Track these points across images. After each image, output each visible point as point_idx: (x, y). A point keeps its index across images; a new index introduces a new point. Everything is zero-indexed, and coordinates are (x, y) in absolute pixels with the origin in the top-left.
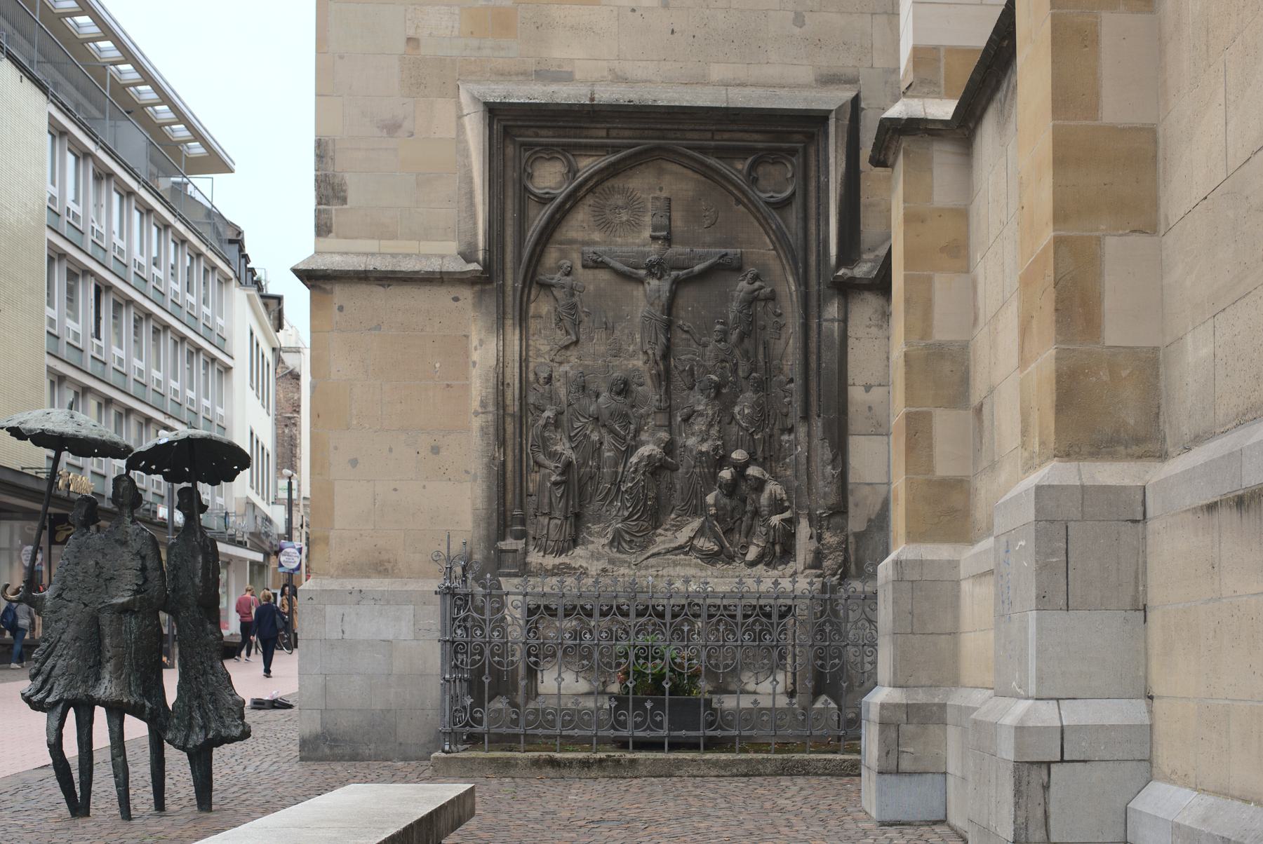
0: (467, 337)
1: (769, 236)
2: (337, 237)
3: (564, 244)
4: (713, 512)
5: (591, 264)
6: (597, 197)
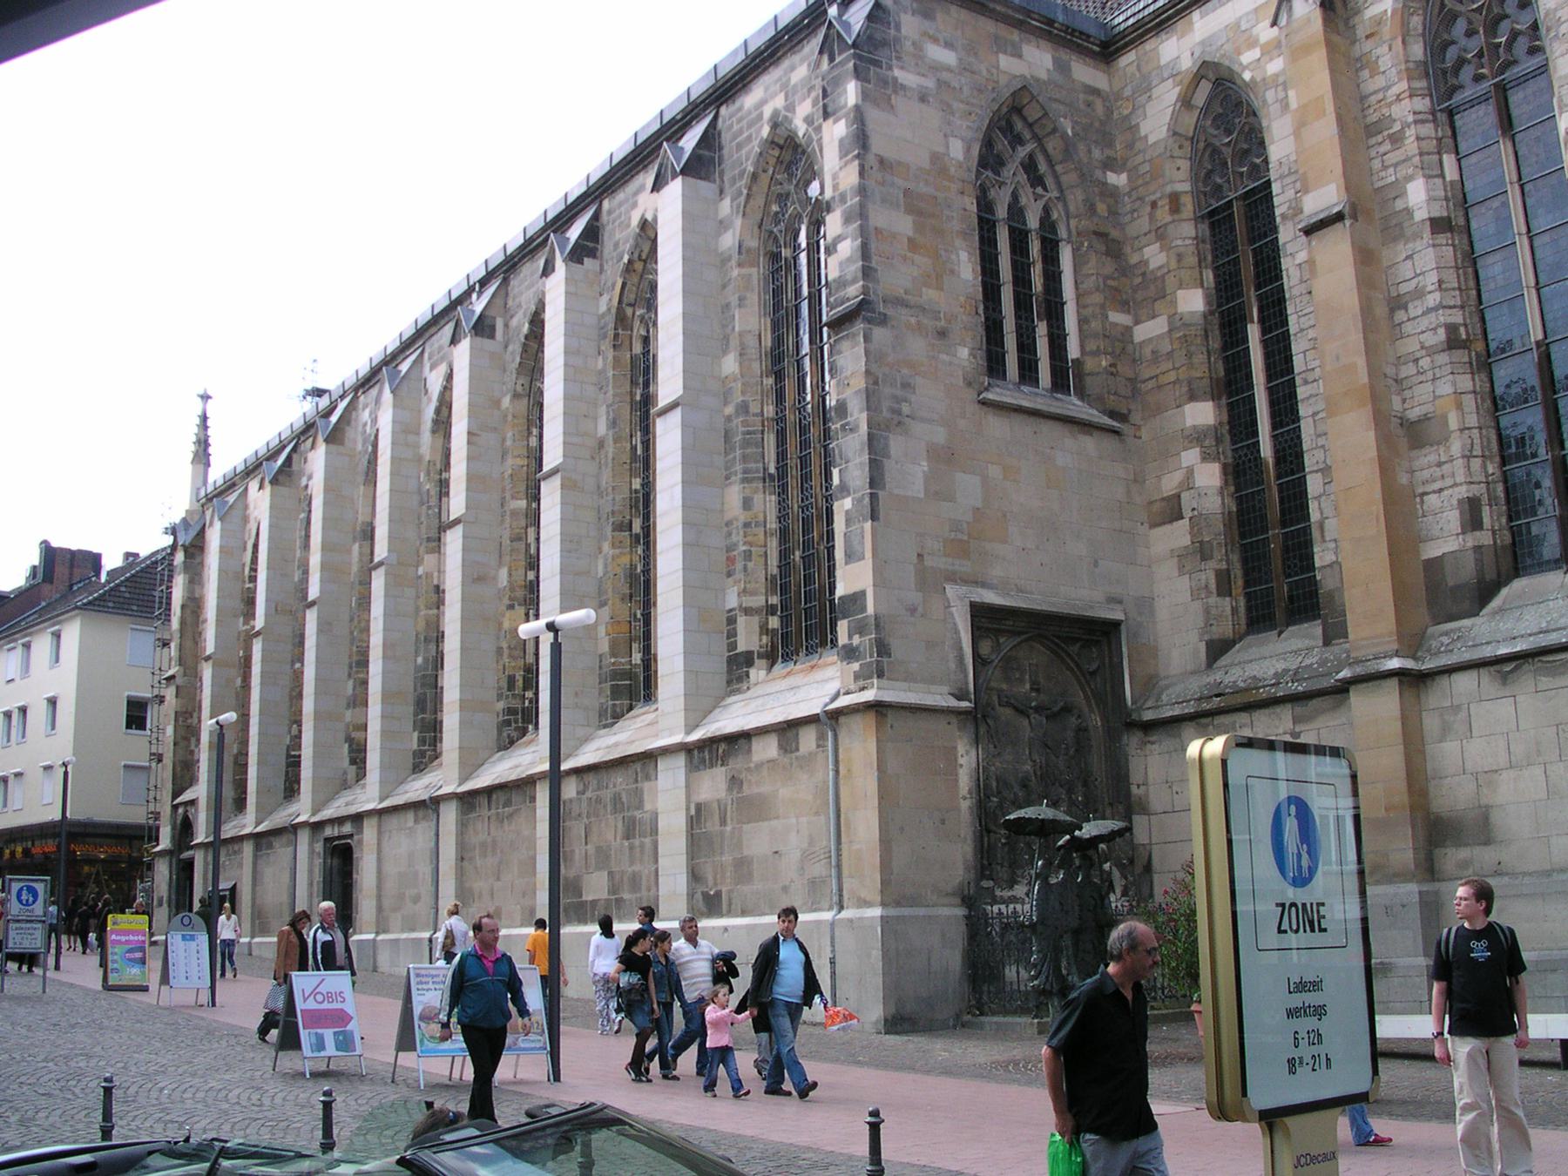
0: (955, 748)
1: (1084, 692)
2: (888, 679)
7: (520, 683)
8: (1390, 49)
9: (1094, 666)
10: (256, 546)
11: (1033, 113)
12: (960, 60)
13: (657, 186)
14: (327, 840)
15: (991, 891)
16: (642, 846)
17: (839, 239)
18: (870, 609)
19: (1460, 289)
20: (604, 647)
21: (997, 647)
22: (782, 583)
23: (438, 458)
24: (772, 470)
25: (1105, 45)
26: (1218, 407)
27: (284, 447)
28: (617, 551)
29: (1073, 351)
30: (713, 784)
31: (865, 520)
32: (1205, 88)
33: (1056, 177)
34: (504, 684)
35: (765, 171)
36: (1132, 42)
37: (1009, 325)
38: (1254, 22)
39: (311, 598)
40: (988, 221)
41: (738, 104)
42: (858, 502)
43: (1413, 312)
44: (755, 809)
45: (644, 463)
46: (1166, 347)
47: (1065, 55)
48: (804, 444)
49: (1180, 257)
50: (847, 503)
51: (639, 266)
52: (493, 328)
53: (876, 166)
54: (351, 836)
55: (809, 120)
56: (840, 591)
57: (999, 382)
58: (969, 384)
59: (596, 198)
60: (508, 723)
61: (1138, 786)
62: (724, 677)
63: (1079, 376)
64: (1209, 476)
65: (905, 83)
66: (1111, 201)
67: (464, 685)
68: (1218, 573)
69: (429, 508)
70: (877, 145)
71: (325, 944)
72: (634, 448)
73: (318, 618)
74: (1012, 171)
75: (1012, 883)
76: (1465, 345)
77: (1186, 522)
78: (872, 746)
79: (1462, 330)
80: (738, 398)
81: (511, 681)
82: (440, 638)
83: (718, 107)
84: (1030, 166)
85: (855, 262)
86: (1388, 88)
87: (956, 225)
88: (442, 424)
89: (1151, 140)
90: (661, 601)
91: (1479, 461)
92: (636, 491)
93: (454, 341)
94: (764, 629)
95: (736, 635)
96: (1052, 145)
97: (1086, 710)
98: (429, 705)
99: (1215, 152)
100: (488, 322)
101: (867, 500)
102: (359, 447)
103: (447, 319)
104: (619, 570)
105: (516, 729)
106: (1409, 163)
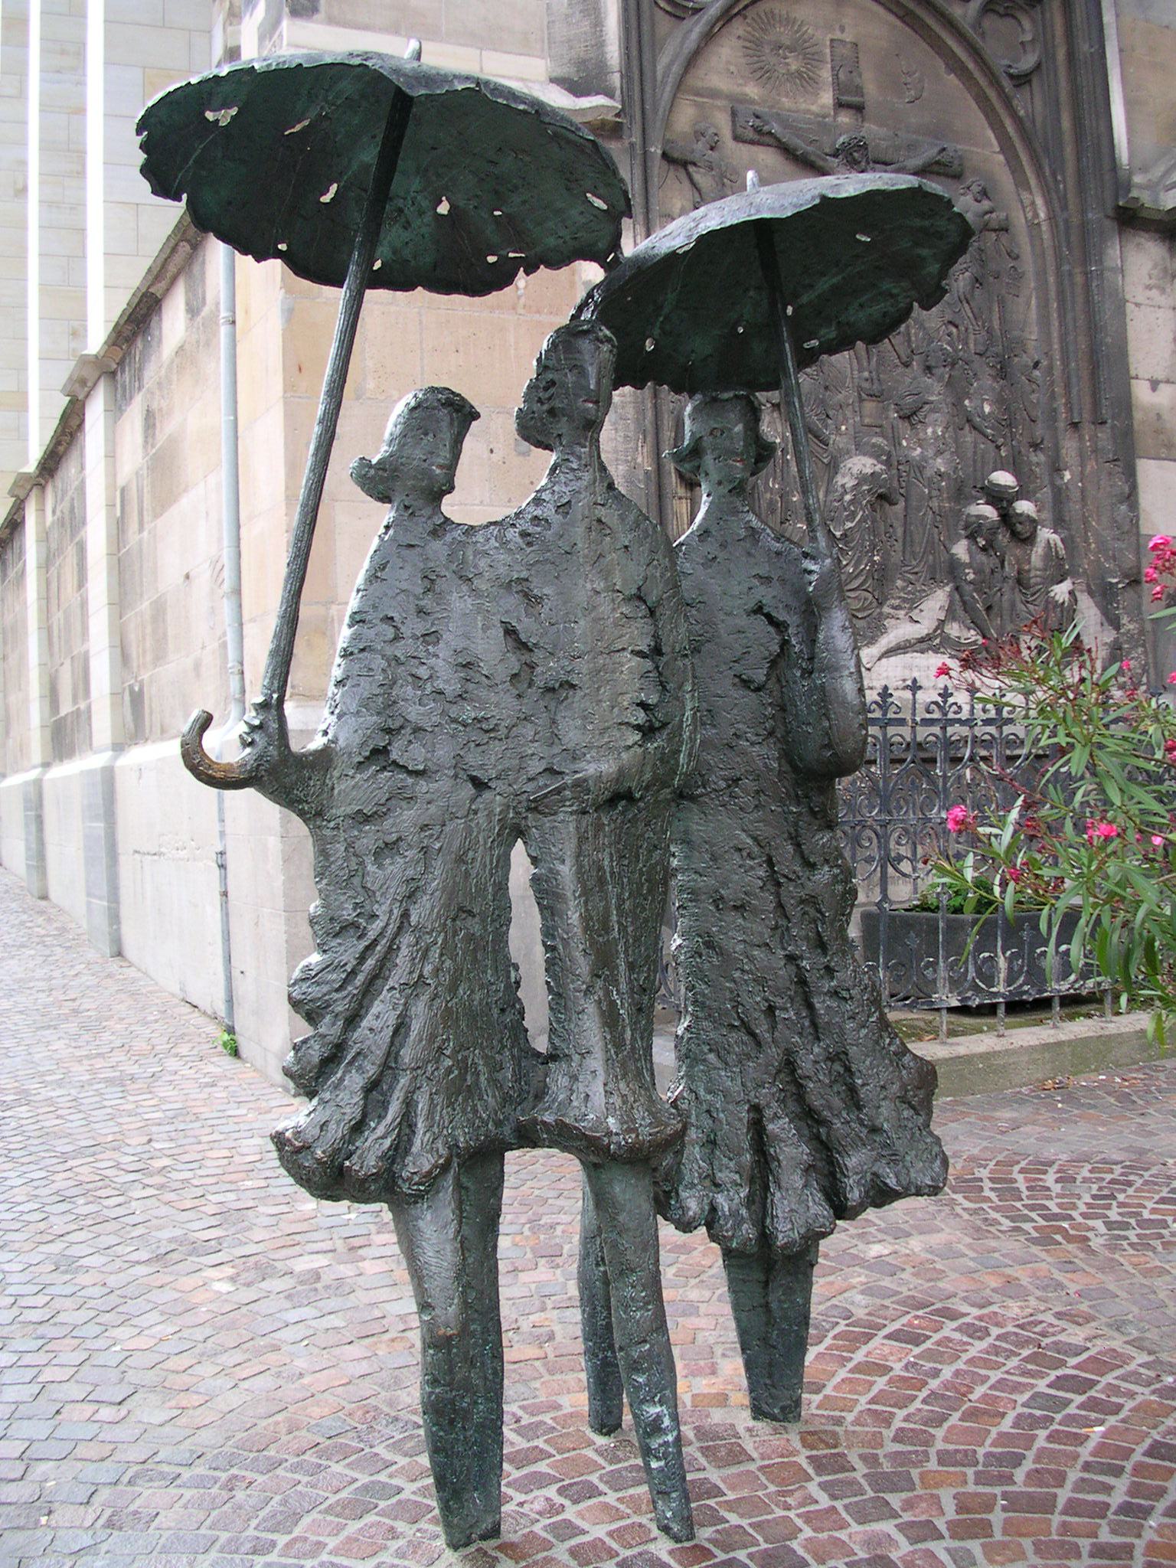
2: (331, 21)
3: (702, 96)
4: (971, 577)
5: (750, 134)
6: (749, 25)
9: (1027, 63)
61: (1154, 385)
71: (940, 1462)
97: (1005, 179)
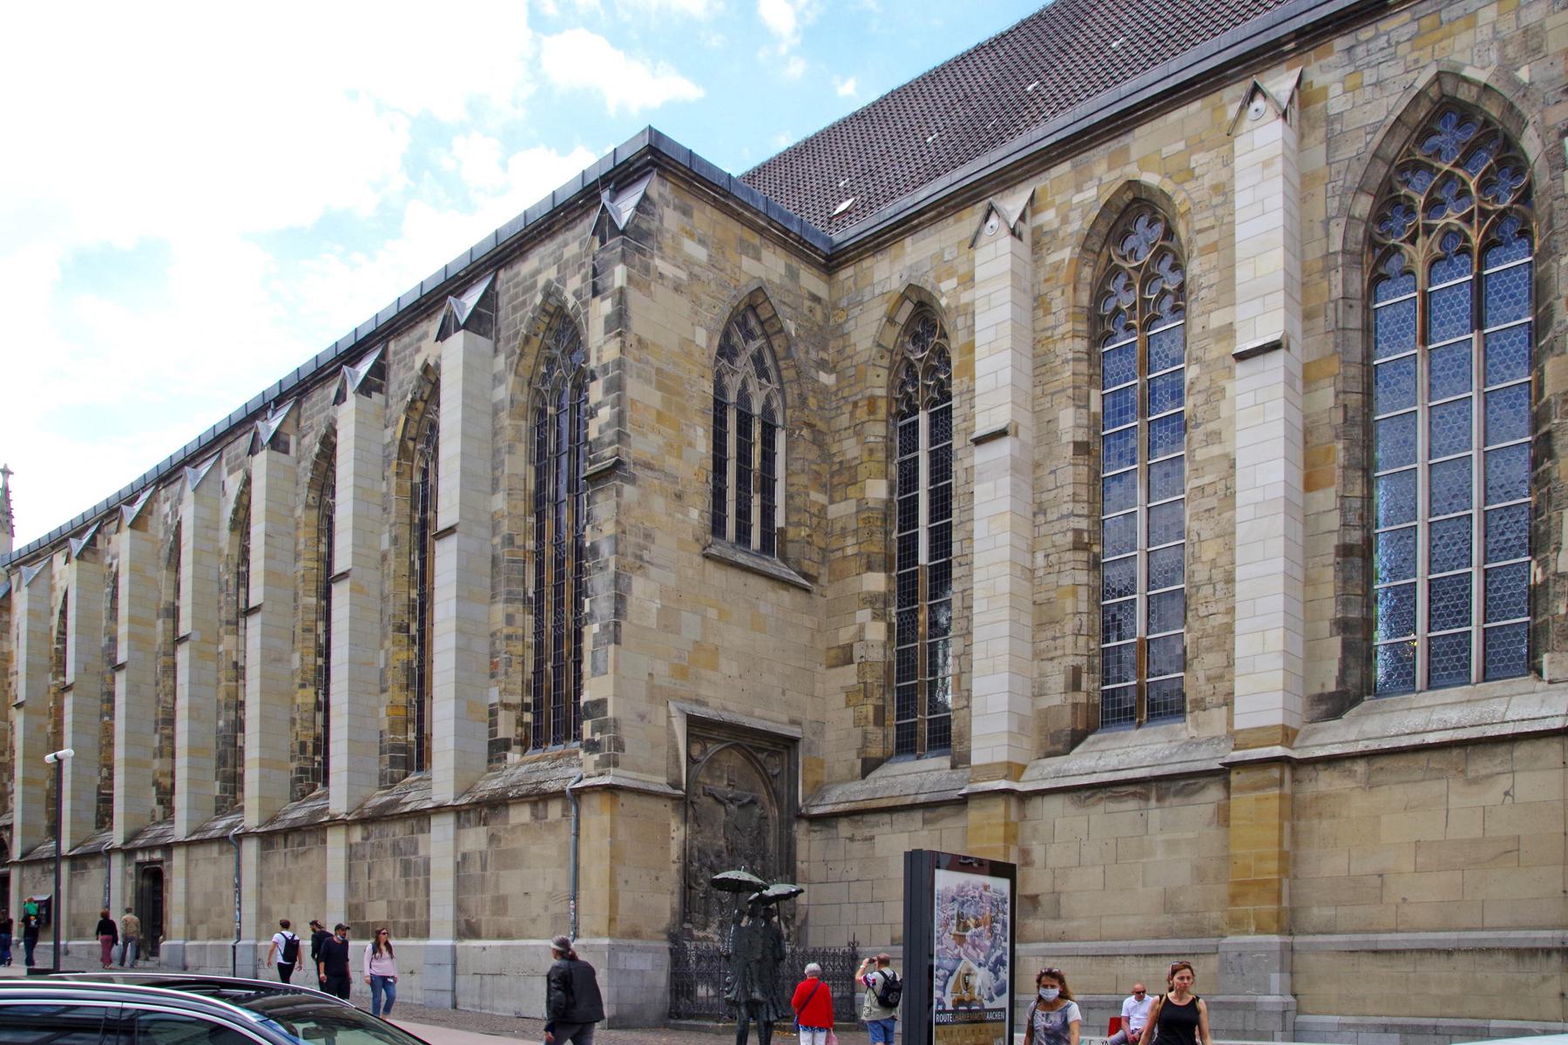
7: (310, 748)
8: (1063, 293)
9: (776, 771)
10: (63, 613)
11: (765, 313)
12: (710, 256)
13: (443, 335)
14: (138, 864)
15: (689, 932)
16: (417, 882)
17: (599, 405)
18: (610, 714)
19: (1088, 502)
20: (385, 725)
21: (704, 751)
22: (535, 685)
23: (236, 552)
24: (531, 594)
25: (829, 258)
26: (889, 578)
27: (88, 527)
28: (397, 649)
29: (779, 521)
30: (476, 838)
31: (609, 643)
32: (908, 307)
33: (778, 370)
34: (297, 748)
35: (536, 335)
36: (852, 258)
37: (731, 494)
38: (955, 254)
39: (120, 660)
40: (722, 403)
41: (516, 268)
42: (605, 627)
43: (1050, 517)
44: (510, 860)
45: (422, 578)
46: (852, 525)
47: (795, 263)
48: (560, 576)
49: (871, 451)
50: (595, 628)
51: (420, 405)
52: (287, 444)
53: (635, 344)
54: (161, 862)
55: (578, 295)
56: (586, 697)
57: (720, 541)
58: (697, 540)
59: (383, 338)
60: (301, 780)
62: (486, 757)
63: (784, 542)
64: (877, 632)
65: (663, 271)
66: (821, 397)
67: (263, 746)
68: (876, 708)
69: (228, 595)
70: (637, 325)
72: (412, 564)
73: (127, 680)
74: (743, 363)
75: (705, 927)
76: (1086, 547)
77: (855, 666)
78: (606, 818)
79: (1086, 535)
80: (505, 528)
81: (303, 746)
82: (241, 705)
83: (498, 270)
84: (758, 359)
85: (613, 427)
86: (1055, 327)
87: (696, 404)
88: (241, 523)
89: (859, 348)
90: (436, 691)
91: (1084, 638)
92: (414, 600)
93: (252, 451)
94: (520, 722)
95: (496, 725)
96: (778, 342)
97: (767, 803)
98: (230, 761)
99: (910, 366)
100: (282, 437)
101: (611, 628)
102: (161, 535)
103: (243, 430)
104: (398, 664)
105: (308, 785)
106: (1063, 394)
